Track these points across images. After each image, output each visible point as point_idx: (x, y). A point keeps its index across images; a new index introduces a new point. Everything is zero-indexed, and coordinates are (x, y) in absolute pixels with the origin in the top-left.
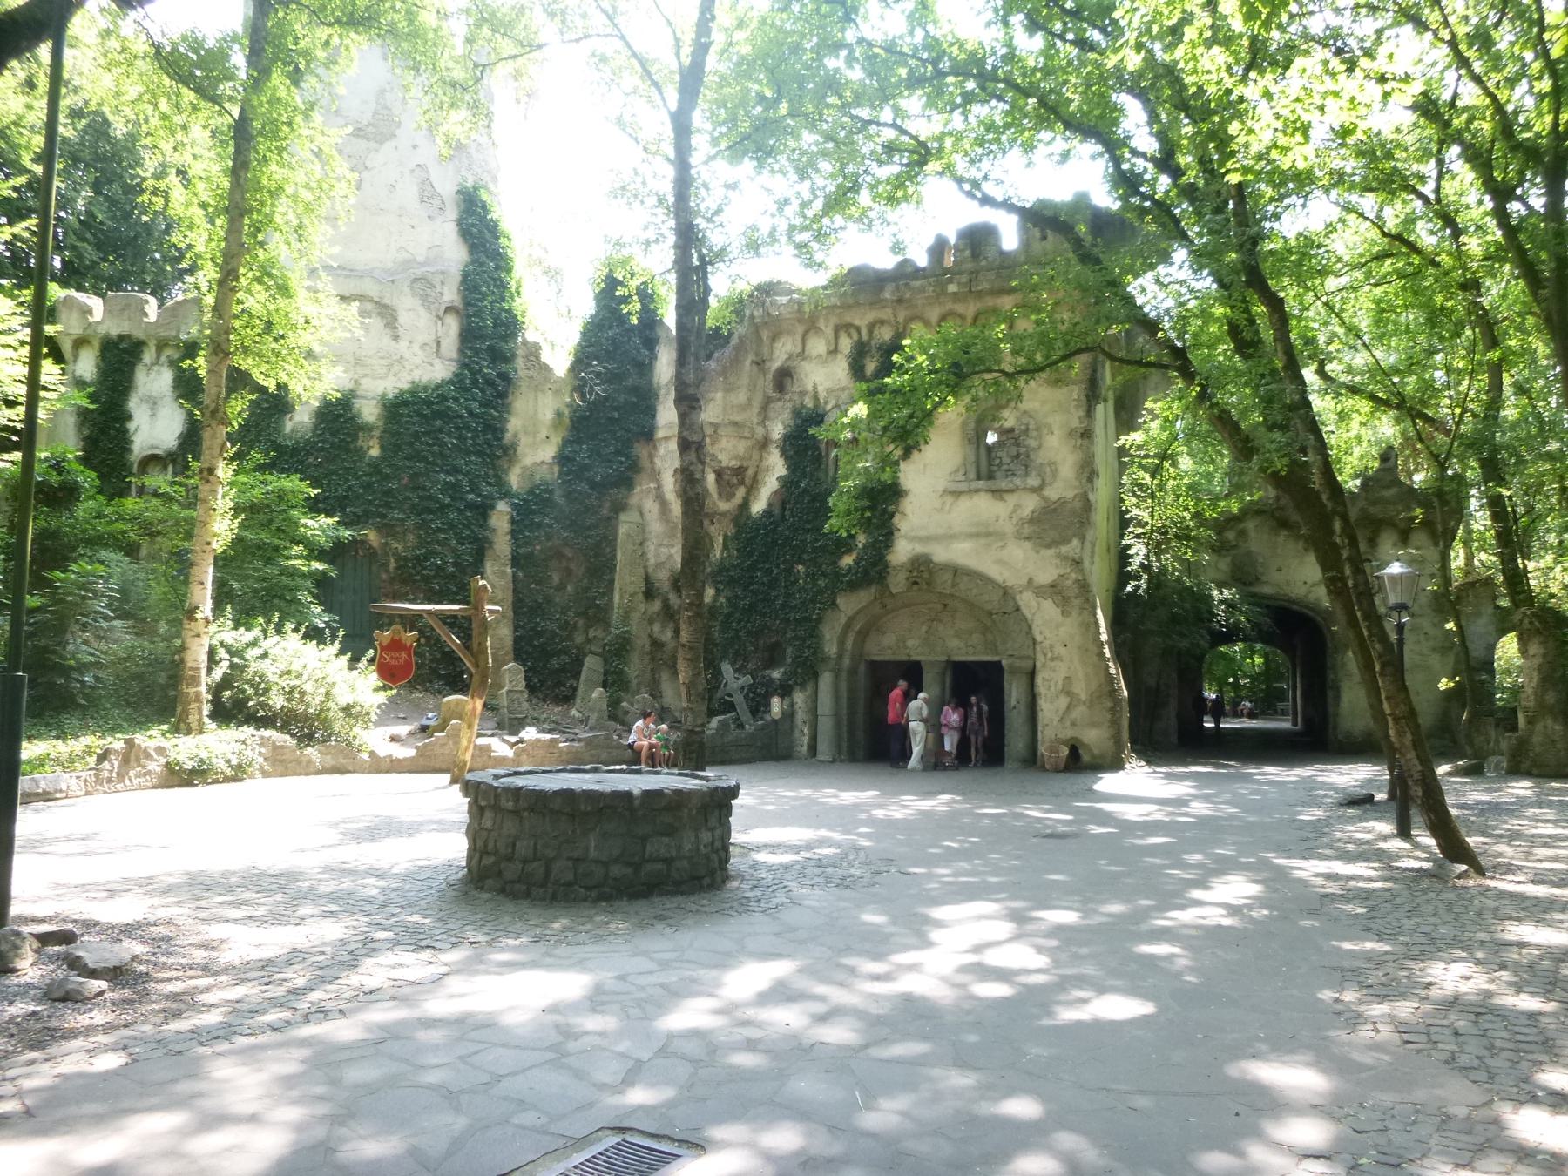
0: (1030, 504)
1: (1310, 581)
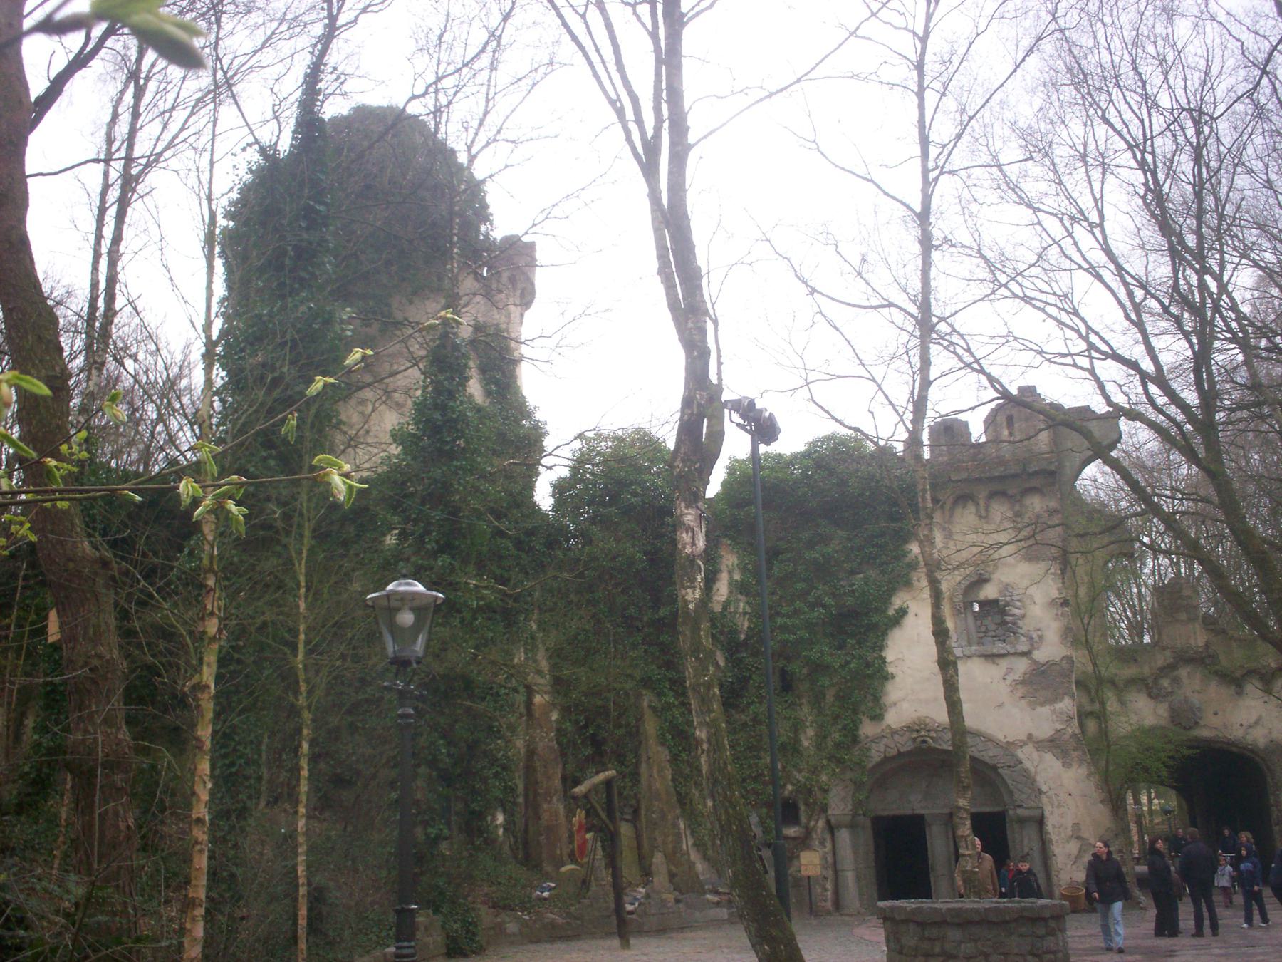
0: (1022, 665)
1: (1245, 723)
